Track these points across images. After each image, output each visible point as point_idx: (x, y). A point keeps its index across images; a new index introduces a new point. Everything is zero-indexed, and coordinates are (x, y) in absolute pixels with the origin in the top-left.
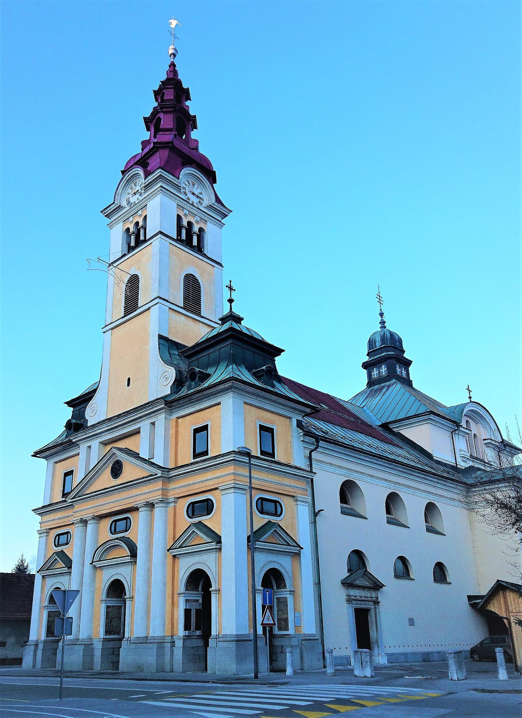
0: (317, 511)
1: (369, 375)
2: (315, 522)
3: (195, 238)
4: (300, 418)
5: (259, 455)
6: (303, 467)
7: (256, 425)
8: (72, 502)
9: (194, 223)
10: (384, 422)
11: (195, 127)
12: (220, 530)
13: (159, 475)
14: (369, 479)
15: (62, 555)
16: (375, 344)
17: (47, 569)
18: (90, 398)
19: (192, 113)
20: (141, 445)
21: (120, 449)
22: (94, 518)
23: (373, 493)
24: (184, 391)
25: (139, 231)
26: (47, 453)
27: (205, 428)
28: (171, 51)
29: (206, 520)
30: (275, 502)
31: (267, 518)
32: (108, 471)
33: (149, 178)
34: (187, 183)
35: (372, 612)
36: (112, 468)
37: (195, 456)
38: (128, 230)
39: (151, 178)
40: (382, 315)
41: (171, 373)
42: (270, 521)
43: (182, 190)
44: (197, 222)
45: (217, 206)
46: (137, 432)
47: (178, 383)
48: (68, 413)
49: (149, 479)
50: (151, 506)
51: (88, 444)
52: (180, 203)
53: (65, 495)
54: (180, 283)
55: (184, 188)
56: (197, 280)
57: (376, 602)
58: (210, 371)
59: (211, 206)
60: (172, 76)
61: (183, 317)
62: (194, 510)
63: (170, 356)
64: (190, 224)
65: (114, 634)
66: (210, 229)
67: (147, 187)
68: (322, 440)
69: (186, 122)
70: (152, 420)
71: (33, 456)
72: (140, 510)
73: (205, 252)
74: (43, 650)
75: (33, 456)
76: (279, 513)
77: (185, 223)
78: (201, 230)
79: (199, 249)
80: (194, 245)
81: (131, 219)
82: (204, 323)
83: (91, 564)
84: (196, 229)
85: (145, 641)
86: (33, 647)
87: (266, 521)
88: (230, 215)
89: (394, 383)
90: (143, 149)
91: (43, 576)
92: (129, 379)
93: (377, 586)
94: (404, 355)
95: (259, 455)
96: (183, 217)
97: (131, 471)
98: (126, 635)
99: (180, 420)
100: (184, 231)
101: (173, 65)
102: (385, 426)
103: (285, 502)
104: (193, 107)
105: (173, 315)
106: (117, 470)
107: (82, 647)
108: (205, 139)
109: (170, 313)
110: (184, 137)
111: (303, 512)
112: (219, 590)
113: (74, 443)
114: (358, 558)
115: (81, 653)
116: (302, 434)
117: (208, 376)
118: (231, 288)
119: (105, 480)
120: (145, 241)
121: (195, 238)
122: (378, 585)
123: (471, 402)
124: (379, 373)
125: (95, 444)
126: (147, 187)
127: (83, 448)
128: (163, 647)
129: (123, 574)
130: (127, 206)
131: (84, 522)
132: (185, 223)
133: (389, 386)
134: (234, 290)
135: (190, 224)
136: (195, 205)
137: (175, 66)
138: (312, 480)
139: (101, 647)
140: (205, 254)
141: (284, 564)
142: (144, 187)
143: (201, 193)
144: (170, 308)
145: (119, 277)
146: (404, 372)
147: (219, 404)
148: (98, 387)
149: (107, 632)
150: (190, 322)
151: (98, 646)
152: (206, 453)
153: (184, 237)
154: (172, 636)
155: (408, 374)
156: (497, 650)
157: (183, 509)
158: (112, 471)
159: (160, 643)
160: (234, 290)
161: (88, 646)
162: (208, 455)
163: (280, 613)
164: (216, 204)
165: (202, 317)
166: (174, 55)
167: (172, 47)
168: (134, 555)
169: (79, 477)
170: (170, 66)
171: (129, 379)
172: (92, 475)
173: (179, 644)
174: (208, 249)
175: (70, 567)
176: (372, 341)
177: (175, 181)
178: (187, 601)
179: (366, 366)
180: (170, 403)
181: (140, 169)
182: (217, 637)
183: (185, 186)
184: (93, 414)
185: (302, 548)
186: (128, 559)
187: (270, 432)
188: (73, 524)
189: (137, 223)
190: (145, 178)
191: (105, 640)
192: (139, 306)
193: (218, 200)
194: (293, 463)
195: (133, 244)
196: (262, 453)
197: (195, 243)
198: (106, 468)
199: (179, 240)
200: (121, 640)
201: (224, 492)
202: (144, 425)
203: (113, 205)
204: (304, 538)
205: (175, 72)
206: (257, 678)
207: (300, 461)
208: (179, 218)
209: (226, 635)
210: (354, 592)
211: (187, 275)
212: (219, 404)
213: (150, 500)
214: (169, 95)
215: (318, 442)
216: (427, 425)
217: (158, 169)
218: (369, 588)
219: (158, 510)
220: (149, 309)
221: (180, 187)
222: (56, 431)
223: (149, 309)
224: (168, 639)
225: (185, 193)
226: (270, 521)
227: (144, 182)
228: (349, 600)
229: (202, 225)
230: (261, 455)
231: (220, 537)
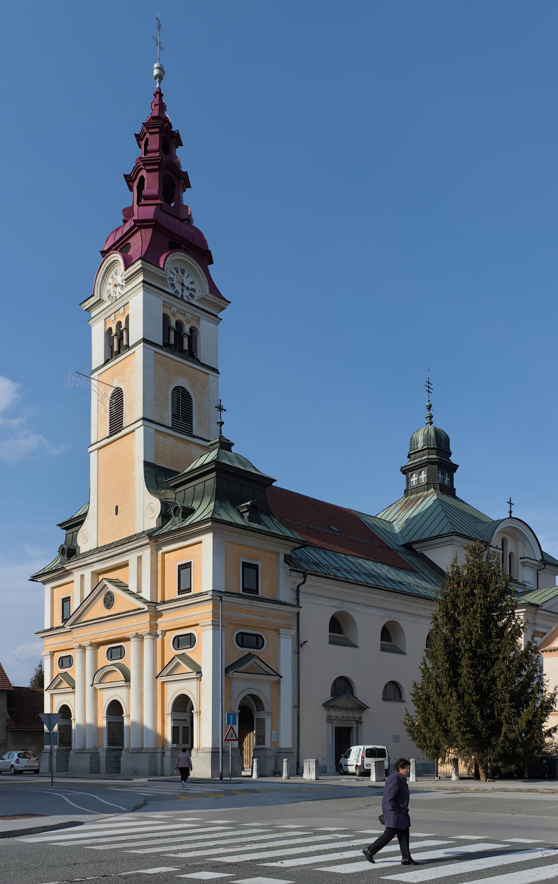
0: (301, 641)
1: (408, 482)
2: (298, 653)
3: (186, 341)
4: (289, 553)
5: (241, 592)
6: (289, 601)
7: (239, 562)
8: (71, 629)
9: (184, 322)
10: (407, 542)
11: (188, 185)
12: (201, 662)
13: (146, 609)
14: (364, 609)
15: (66, 676)
16: (417, 444)
17: (54, 689)
18: (81, 523)
19: (183, 169)
20: (129, 577)
21: (110, 581)
22: (91, 644)
23: (368, 624)
24: (169, 527)
25: (122, 332)
26: (44, 578)
27: (188, 565)
28: (156, 72)
29: (188, 652)
30: (257, 636)
31: (247, 651)
32: (100, 601)
33: (130, 269)
34: (174, 272)
35: (354, 731)
36: (105, 599)
37: (180, 592)
38: (110, 329)
39: (132, 269)
40: (429, 407)
41: (156, 505)
42: (250, 653)
43: (169, 282)
44: (174, 314)
45: (211, 298)
46: (125, 565)
47: (164, 517)
48: (60, 537)
49: (137, 612)
50: (140, 637)
51: (82, 572)
52: (166, 300)
53: (64, 620)
54: (167, 398)
55: (172, 279)
56: (188, 393)
57: (359, 722)
58: (195, 505)
59: (205, 298)
60: (156, 114)
61: (172, 439)
62: (178, 642)
63: (157, 485)
64: (179, 324)
65: (117, 745)
66: (205, 327)
67: (128, 280)
68: (309, 574)
69: (174, 180)
70: (139, 554)
71: (30, 580)
72: (132, 640)
73: (198, 357)
74: (57, 757)
75: (30, 580)
76: (260, 646)
77: (173, 324)
78: (192, 330)
79: (191, 354)
80: (184, 349)
81: (113, 317)
82: (195, 443)
83: (91, 686)
84: (187, 330)
85: (140, 751)
86: (48, 755)
87: (246, 653)
88: (229, 307)
89: (431, 493)
90: (125, 222)
91: (51, 695)
92: (117, 507)
93: (362, 708)
94: (450, 458)
95: (241, 592)
96: (170, 316)
97: (123, 603)
98: (126, 746)
99: (166, 555)
100: (172, 334)
101: (159, 94)
102: (408, 547)
103: (267, 636)
104: (184, 157)
105: (160, 438)
106: (109, 601)
107: (89, 755)
108: (199, 204)
109: (157, 435)
110: (172, 205)
111: (286, 645)
112: (200, 712)
113: (67, 571)
114: (343, 686)
115: (88, 760)
116: (288, 569)
117: (193, 511)
118: (220, 408)
119: (98, 609)
120: (128, 347)
121: (186, 341)
122: (363, 708)
123: (511, 517)
124: (418, 480)
125: (87, 573)
126: (128, 280)
127: (76, 576)
128: (156, 756)
129: (120, 695)
130: (108, 300)
131: (82, 648)
132: (173, 324)
133: (426, 497)
134: (225, 410)
135: (179, 324)
136: (185, 298)
137: (161, 95)
138: (298, 614)
139: (105, 755)
140: (197, 359)
141: (263, 690)
142: (126, 280)
143: (192, 283)
144: (156, 430)
145: (103, 394)
146: (447, 479)
147: (201, 542)
148: (88, 510)
149: (109, 743)
150: (180, 445)
151: (103, 755)
152: (189, 590)
153: (172, 341)
154: (163, 748)
155: (452, 481)
156: (285, 760)
157: (170, 641)
158: (105, 602)
159: (152, 753)
160: (225, 410)
161: (94, 754)
162: (191, 592)
163: (259, 731)
164: (210, 295)
165: (194, 437)
166: (160, 77)
167: (156, 65)
168: (127, 679)
169: (75, 604)
170: (155, 95)
171: (117, 507)
172: (87, 604)
173: (168, 754)
174: (203, 354)
175: (74, 688)
176: (414, 441)
177: (160, 273)
178: (174, 720)
179: (406, 471)
180: (156, 538)
181: (119, 256)
182: (128, 750)
183: (172, 276)
184: (87, 539)
185: (281, 677)
186: (123, 683)
187: (254, 569)
188: (73, 649)
189: (119, 324)
190: (126, 268)
191: (108, 750)
192: (124, 426)
193: (213, 289)
194: (282, 599)
195: (115, 349)
196: (244, 589)
197: (186, 347)
198: (99, 598)
199: (166, 345)
200: (122, 750)
201: (204, 628)
202: (132, 558)
203: (93, 298)
204: (286, 668)
205: (162, 107)
206: (118, 770)
207: (286, 595)
208: (165, 317)
209: (204, 748)
210: (334, 713)
211: (175, 388)
212: (201, 542)
213: (140, 632)
214: (154, 142)
215: (305, 577)
216: (450, 547)
217: (138, 260)
218: (353, 709)
219: (147, 642)
220: (134, 431)
221: (166, 279)
222: (49, 558)
223: (134, 431)
224: (159, 750)
225: (173, 285)
226: (250, 653)
227: (125, 273)
228: (329, 719)
229: (194, 324)
230: (243, 591)
231: (200, 668)
